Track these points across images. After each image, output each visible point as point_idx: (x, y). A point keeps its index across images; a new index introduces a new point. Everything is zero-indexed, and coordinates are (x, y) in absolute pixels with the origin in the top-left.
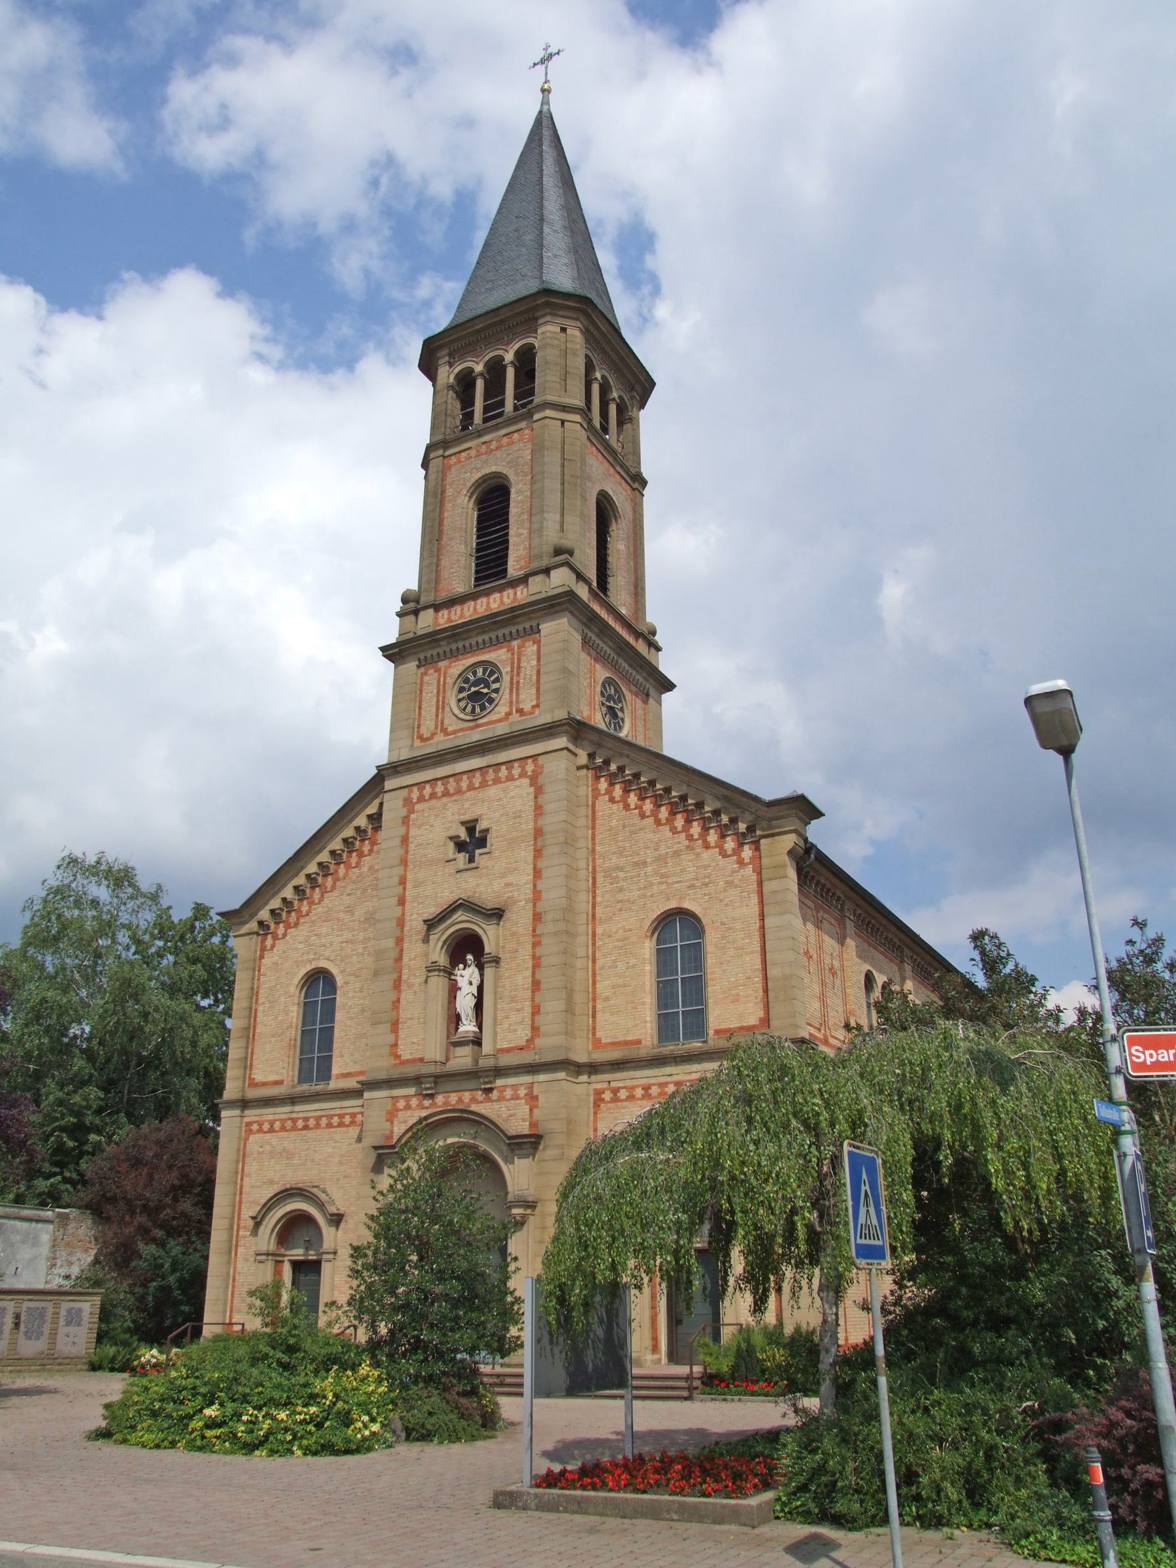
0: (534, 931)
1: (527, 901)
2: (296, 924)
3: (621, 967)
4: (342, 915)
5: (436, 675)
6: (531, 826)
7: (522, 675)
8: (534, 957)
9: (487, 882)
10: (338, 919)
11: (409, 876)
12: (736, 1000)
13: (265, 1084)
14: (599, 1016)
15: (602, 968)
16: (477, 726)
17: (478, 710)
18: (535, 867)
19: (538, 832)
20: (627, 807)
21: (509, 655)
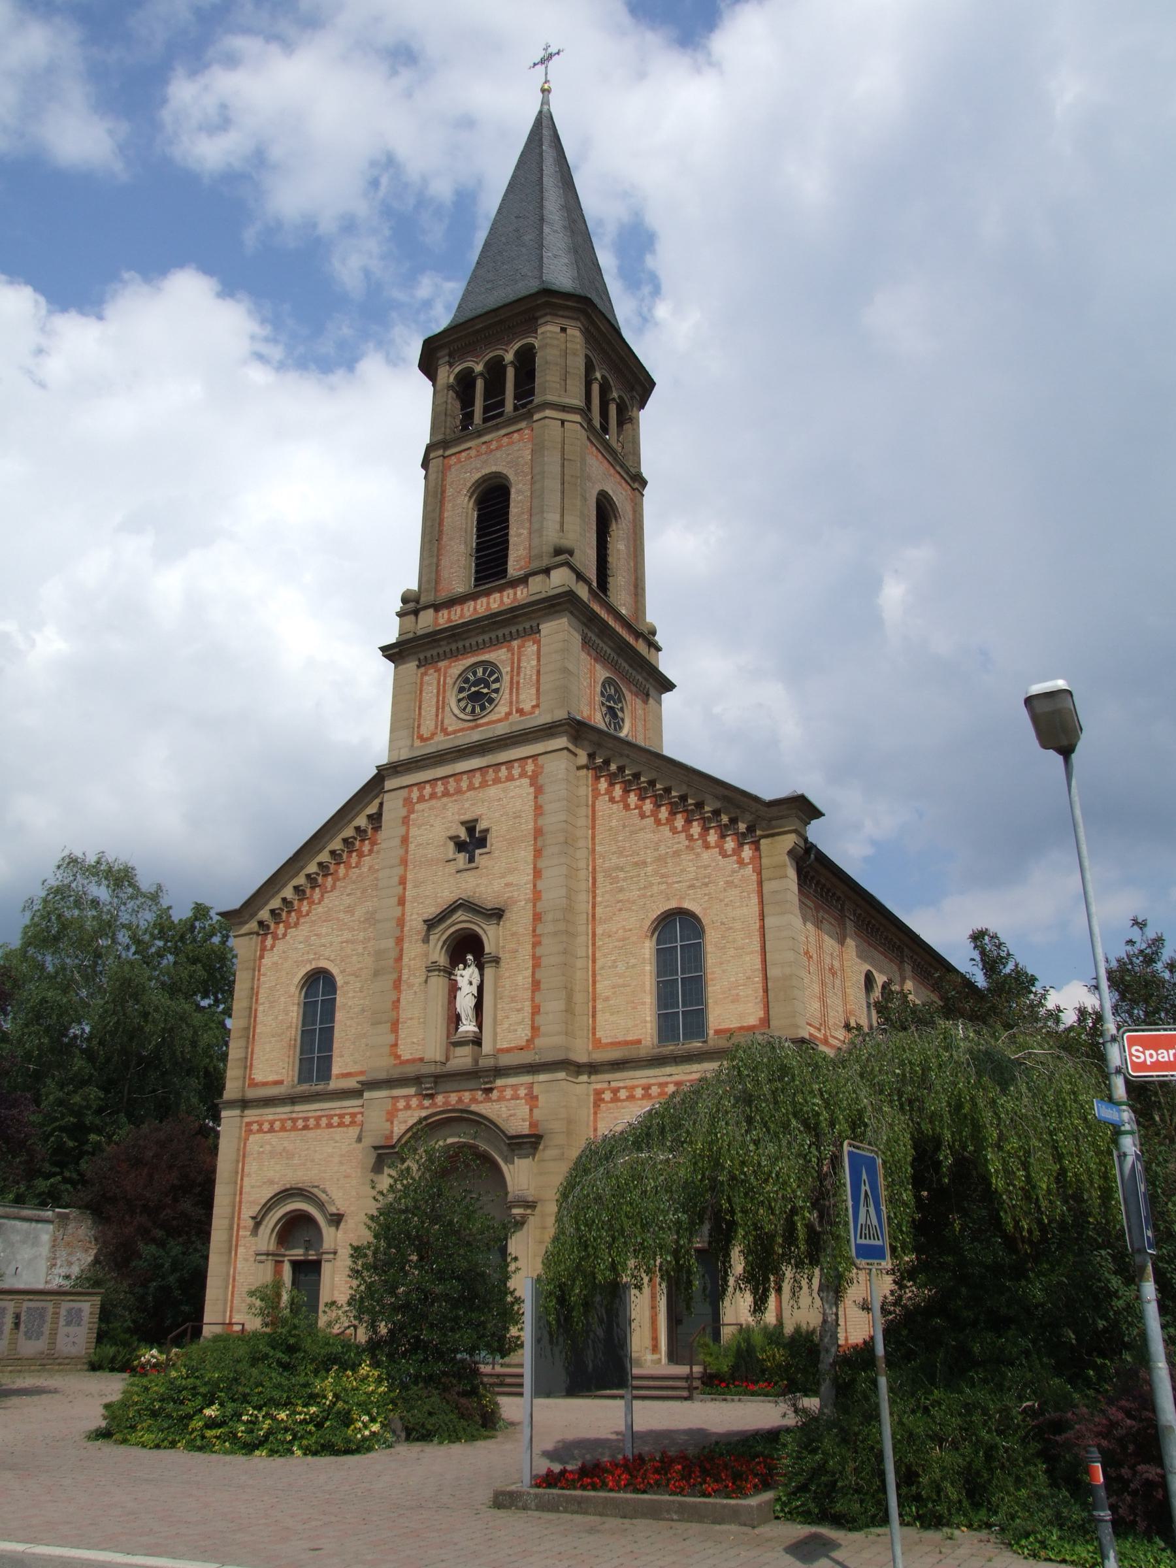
0: (534, 931)
1: (527, 901)
2: (296, 924)
3: (621, 967)
4: (342, 915)
5: (436, 674)
6: (531, 825)
7: (522, 675)
8: (534, 957)
9: (488, 881)
10: (338, 919)
11: (409, 876)
12: (736, 1000)
13: (265, 1084)
14: (599, 1016)
15: (603, 968)
16: (477, 726)
17: (478, 709)
18: (535, 867)
19: (538, 832)
20: (627, 807)
21: (510, 655)
